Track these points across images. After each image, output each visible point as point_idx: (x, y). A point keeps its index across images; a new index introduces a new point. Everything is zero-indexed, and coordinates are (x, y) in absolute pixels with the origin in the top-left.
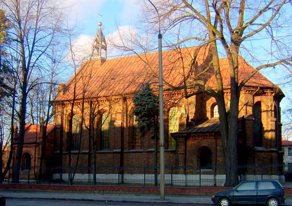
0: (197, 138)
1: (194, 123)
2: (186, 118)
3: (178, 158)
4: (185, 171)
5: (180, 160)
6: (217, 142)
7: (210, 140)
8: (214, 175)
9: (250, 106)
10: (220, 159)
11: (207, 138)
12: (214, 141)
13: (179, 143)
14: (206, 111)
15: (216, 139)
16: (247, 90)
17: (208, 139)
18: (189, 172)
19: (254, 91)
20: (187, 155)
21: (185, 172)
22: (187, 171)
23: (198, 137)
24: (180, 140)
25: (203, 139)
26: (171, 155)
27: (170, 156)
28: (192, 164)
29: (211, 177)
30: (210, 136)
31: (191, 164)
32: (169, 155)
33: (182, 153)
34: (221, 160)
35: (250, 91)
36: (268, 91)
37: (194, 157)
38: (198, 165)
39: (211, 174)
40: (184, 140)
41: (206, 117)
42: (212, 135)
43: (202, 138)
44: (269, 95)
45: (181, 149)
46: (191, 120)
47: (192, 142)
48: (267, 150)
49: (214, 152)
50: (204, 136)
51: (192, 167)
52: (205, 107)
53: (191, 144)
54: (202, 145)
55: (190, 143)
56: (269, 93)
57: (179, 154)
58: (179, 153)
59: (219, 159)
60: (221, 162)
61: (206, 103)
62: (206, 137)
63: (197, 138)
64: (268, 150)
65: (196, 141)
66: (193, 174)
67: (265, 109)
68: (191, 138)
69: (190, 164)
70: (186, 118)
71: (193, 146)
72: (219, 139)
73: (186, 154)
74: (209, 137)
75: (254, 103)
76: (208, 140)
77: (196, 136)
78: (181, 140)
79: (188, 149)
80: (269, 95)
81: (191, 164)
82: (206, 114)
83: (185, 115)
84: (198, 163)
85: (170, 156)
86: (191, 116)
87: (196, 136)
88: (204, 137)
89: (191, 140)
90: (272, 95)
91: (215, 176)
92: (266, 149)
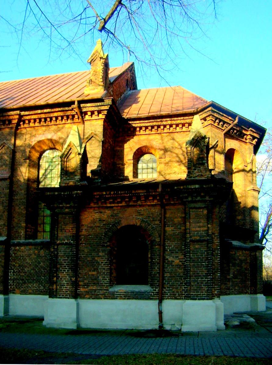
0: (110, 203)
1: (97, 179)
2: (80, 156)
3: (57, 256)
4: (76, 289)
5: (61, 259)
6: (165, 213)
7: (145, 208)
8: (157, 301)
9: (220, 153)
10: (175, 259)
11: (139, 203)
12: (156, 211)
13: (60, 216)
14: (123, 165)
15: (163, 206)
16: (217, 118)
17: (141, 206)
18: (87, 293)
19: (228, 123)
20: (81, 247)
21: (76, 291)
22: (82, 290)
23: (113, 203)
24: (62, 208)
25: (128, 206)
26: (42, 252)
27: (39, 256)
28: (95, 273)
29: (151, 306)
30: (147, 198)
31: (94, 273)
32: (36, 252)
33: (66, 244)
34: (177, 261)
35: (221, 123)
36: (248, 133)
37: (100, 254)
38: (111, 274)
39: (149, 298)
40: (79, 265)
41: (124, 176)
42: (153, 196)
43: (124, 204)
44: (247, 141)
45: (66, 232)
46: (93, 172)
47: (97, 216)
48: (245, 245)
49: (158, 240)
50: (130, 198)
51: (95, 281)
52: (120, 156)
53: (94, 222)
54: (124, 223)
55: (91, 217)
56: (249, 137)
57: (58, 245)
58: (58, 242)
59: (170, 259)
60: (178, 266)
61: (123, 147)
62: (137, 201)
63: (109, 205)
64: (247, 246)
65: (108, 212)
66: (97, 297)
67: (241, 167)
68: (92, 205)
69: (90, 273)
70: (79, 154)
71: (98, 224)
72: (171, 207)
73: (77, 245)
74: (145, 201)
75: (226, 150)
76: (142, 208)
77: (106, 199)
78: (67, 208)
79: (84, 232)
80: (247, 141)
81: (94, 273)
82: (122, 171)
83: (79, 148)
84: (111, 269)
85: (39, 256)
86: (93, 165)
87: (109, 198)
88: (129, 201)
89: (92, 210)
90: (252, 142)
91: (160, 302)
92: (245, 244)
